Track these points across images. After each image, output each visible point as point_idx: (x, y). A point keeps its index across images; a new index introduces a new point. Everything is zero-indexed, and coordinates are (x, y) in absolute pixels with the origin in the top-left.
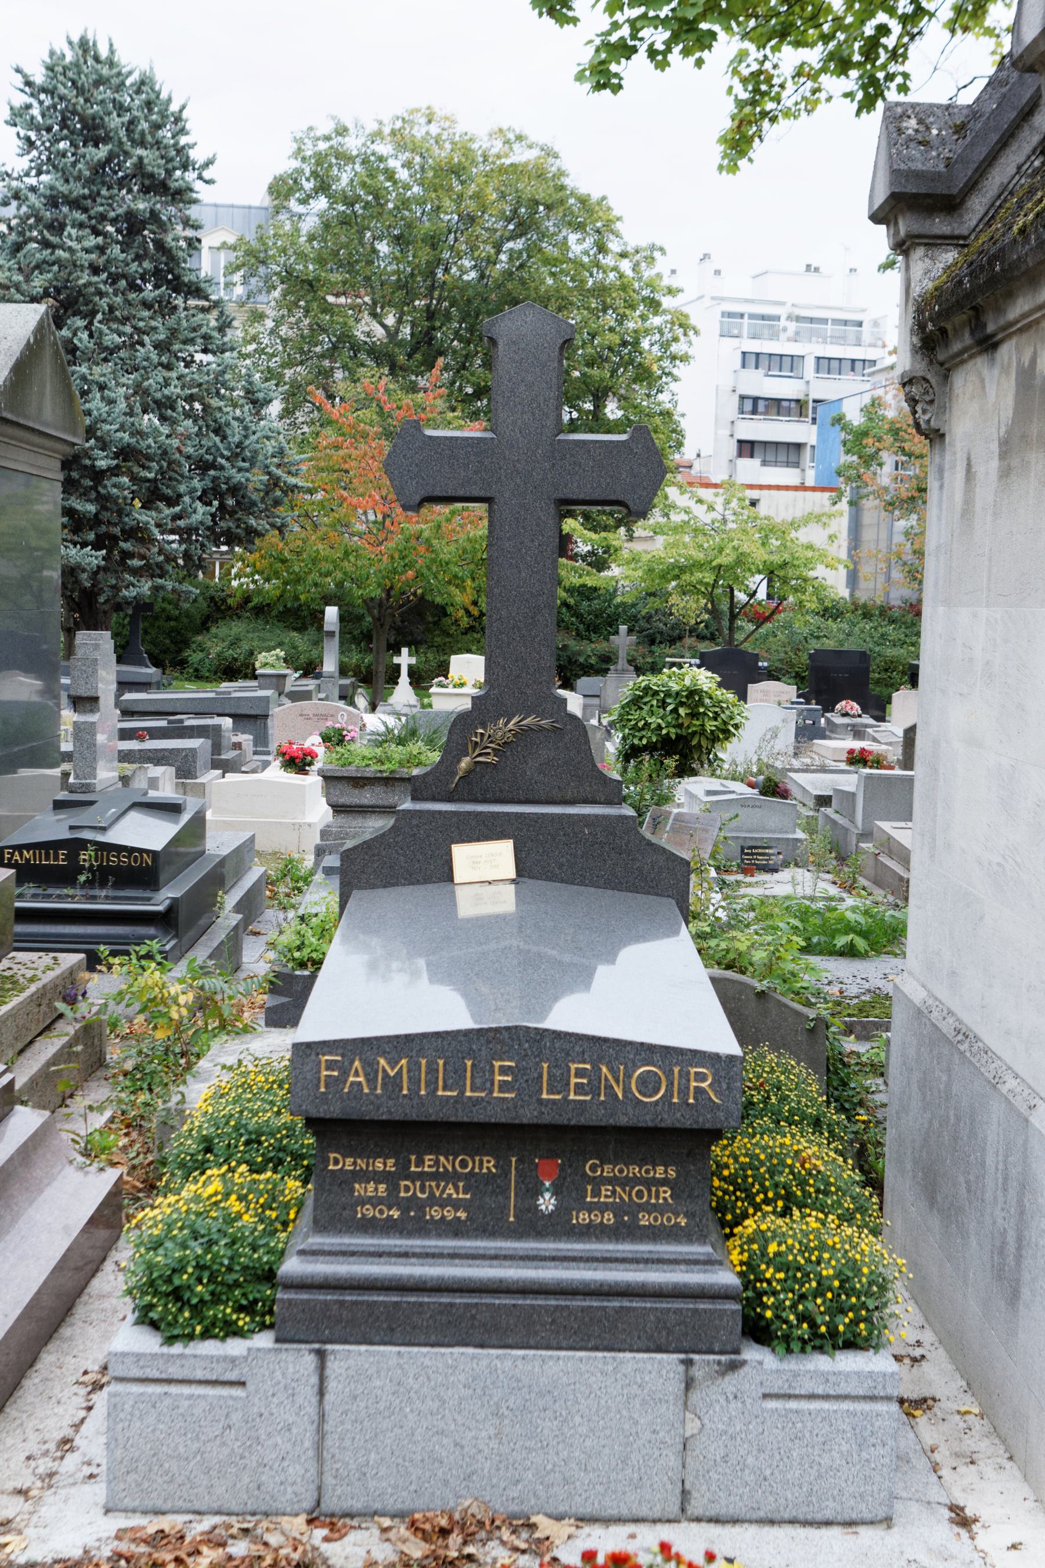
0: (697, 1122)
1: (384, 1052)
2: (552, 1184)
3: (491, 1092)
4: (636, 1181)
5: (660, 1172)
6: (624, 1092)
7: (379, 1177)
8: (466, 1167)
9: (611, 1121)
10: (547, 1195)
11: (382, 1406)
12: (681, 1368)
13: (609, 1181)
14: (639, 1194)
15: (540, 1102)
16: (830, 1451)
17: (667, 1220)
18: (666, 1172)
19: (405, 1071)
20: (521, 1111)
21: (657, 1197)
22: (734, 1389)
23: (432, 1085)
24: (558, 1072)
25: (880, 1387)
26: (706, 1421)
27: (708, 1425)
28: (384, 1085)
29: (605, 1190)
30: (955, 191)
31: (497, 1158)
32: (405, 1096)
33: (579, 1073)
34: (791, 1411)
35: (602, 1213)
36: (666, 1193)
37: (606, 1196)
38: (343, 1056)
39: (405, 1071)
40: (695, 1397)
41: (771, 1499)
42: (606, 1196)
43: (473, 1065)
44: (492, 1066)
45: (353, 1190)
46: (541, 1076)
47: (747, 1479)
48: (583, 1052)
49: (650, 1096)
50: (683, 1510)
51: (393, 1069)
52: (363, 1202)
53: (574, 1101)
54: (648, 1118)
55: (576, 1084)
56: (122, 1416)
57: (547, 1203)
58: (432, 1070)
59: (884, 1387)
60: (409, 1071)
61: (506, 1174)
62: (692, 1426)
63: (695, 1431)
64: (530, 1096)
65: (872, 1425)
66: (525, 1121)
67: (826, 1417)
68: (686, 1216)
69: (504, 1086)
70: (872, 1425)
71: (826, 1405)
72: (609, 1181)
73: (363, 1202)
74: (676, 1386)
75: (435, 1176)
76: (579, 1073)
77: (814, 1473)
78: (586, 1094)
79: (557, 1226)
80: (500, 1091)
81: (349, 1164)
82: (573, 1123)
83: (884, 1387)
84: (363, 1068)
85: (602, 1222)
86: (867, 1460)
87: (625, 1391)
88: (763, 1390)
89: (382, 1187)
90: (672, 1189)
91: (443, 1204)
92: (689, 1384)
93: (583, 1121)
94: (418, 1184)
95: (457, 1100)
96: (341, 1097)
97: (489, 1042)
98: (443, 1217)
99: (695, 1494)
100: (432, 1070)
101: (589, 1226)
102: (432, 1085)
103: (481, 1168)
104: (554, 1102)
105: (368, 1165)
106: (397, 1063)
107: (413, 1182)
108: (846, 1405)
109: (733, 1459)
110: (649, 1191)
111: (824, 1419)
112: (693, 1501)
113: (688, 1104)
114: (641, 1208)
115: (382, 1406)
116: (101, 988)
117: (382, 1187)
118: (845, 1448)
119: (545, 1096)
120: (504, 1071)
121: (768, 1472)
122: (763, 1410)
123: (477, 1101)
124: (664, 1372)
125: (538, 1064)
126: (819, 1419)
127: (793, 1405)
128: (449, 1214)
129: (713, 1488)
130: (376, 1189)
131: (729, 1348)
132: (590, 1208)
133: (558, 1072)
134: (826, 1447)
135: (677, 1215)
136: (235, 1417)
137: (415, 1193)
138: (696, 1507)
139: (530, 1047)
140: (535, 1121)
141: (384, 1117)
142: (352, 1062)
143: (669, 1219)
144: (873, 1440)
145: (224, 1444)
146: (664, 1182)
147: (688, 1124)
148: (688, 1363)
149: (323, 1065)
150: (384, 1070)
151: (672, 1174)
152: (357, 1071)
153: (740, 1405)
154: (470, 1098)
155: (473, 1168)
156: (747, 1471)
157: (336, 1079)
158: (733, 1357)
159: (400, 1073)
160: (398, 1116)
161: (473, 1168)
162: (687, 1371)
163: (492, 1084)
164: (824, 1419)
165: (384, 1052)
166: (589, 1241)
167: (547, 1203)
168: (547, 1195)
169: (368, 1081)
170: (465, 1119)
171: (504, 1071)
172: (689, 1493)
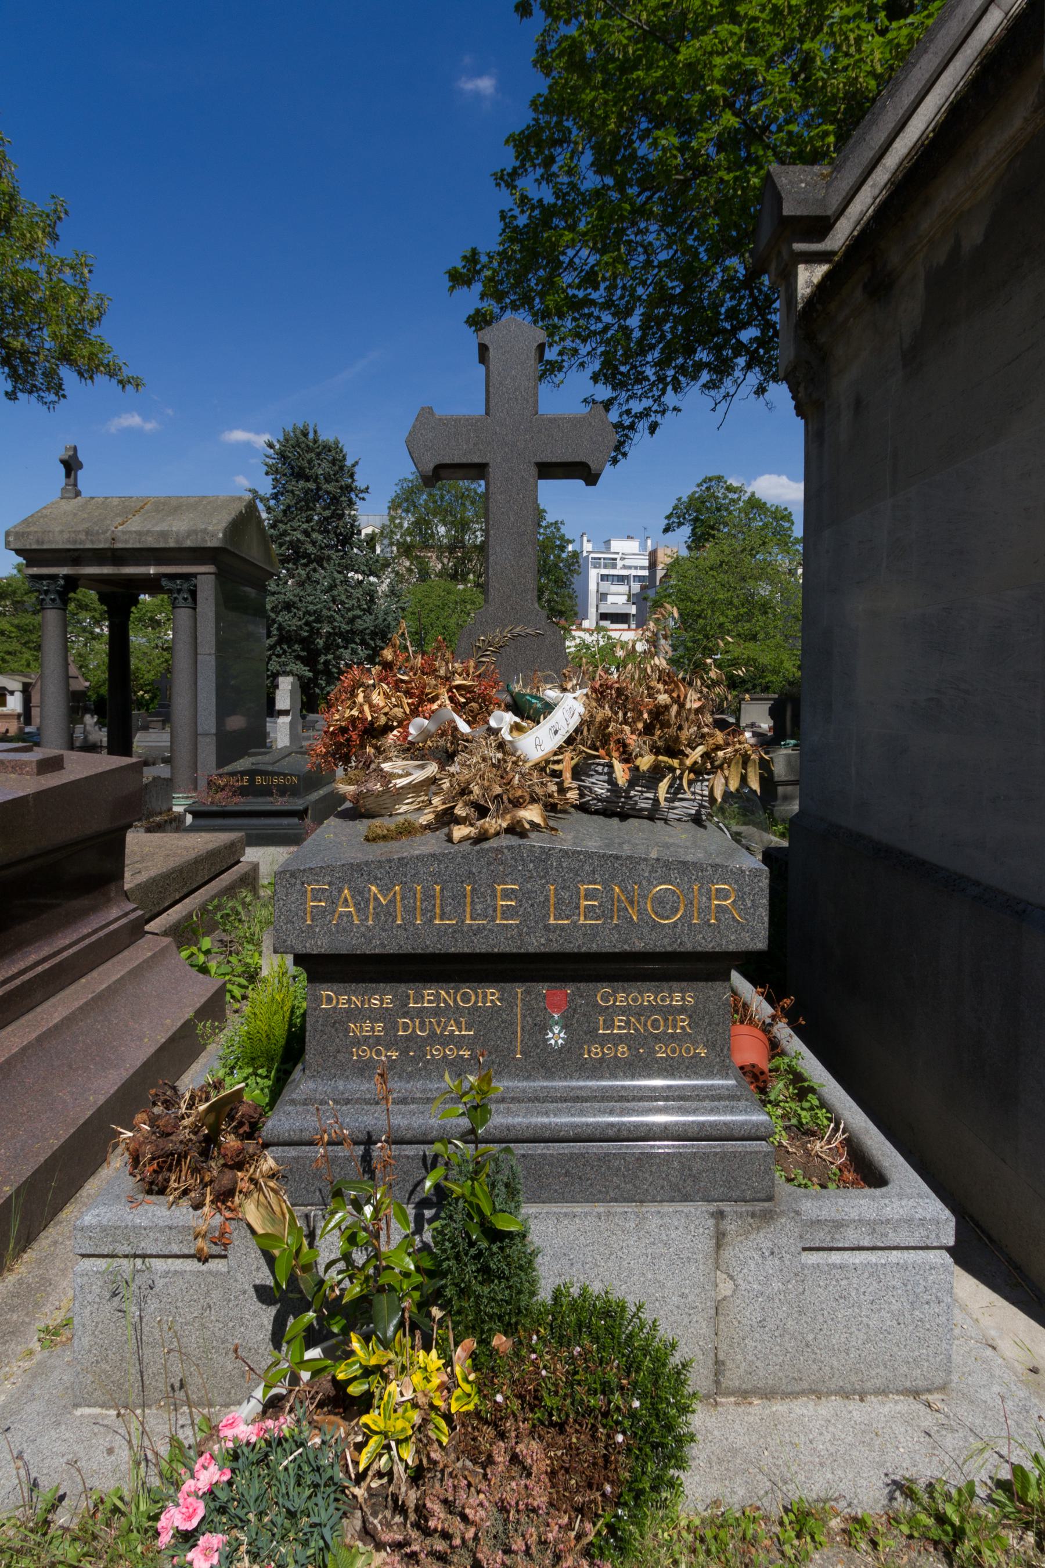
0: (721, 945)
1: (376, 878)
2: (562, 1017)
3: (494, 919)
4: (654, 1009)
5: (677, 1000)
6: (640, 913)
7: (375, 1015)
8: (469, 1001)
9: (626, 947)
10: (556, 1029)
11: (675, 287)
12: (711, 1222)
13: (623, 1011)
14: (655, 1024)
15: (547, 927)
16: (879, 1310)
17: (688, 1050)
18: (683, 999)
19: (398, 897)
20: (527, 939)
21: (675, 1027)
22: (770, 1244)
23: (429, 914)
24: (566, 895)
25: (933, 1236)
26: (740, 1282)
27: (743, 1285)
28: (377, 915)
29: (619, 1020)
30: (829, 213)
31: (502, 991)
32: (399, 926)
33: (590, 895)
34: (834, 1266)
35: (616, 1045)
36: (684, 1021)
37: (619, 1027)
38: (330, 884)
39: (398, 897)
40: (727, 1253)
41: (815, 1367)
42: (619, 1027)
43: (473, 890)
44: (494, 890)
45: (347, 1030)
46: (547, 900)
47: (788, 1345)
48: (593, 872)
49: (667, 918)
50: (717, 1383)
51: (385, 896)
52: (357, 1042)
53: (584, 925)
54: (666, 941)
55: (586, 907)
56: (89, 1298)
57: (556, 1037)
58: (428, 896)
59: (938, 1237)
60: (402, 899)
61: (512, 1006)
62: (726, 1288)
63: (729, 1293)
64: (536, 922)
65: (926, 1280)
66: (531, 950)
67: (874, 1271)
68: (706, 1046)
69: (507, 912)
70: (926, 1280)
71: (872, 1257)
72: (623, 1011)
73: (357, 1042)
74: (706, 1244)
75: (437, 1012)
76: (590, 895)
77: (862, 1336)
78: (597, 918)
79: (566, 1062)
80: (502, 919)
81: (343, 1002)
82: (583, 950)
83: (938, 1237)
84: (353, 897)
85: (616, 1056)
86: (921, 1320)
87: (650, 1251)
88: (802, 1245)
89: (379, 1026)
90: (690, 1017)
91: (447, 1041)
92: (720, 1239)
93: (594, 948)
94: (417, 1021)
95: (457, 929)
96: (330, 930)
97: (489, 864)
98: (445, 1056)
99: (729, 1364)
100: (428, 896)
101: (602, 1060)
102: (429, 914)
103: (484, 1003)
104: (562, 928)
105: (363, 1003)
106: (389, 890)
107: (411, 1019)
108: (895, 1256)
109: (771, 1325)
110: (666, 1020)
111: (871, 1275)
112: (727, 1374)
113: (710, 925)
114: (657, 1038)
115: (675, 287)
116: (252, 854)
117: (379, 1026)
118: (896, 1306)
119: (552, 921)
120: (507, 895)
121: (810, 1337)
122: (803, 1267)
123: (478, 931)
124: (692, 1227)
125: (543, 886)
126: (866, 1275)
127: (835, 1257)
128: (450, 1053)
129: (750, 1358)
130: (373, 1029)
131: (762, 1195)
132: (603, 1040)
133: (566, 895)
134: (875, 1307)
135: (695, 1043)
136: (216, 1295)
137: (414, 1031)
138: (732, 1379)
139: (536, 868)
140: (543, 949)
141: (377, 951)
142: (340, 891)
143: (688, 1050)
144: (927, 1297)
145: (203, 1326)
146: (682, 1010)
147: (709, 947)
148: (720, 1215)
149: (309, 895)
150: (376, 899)
151: (690, 1000)
152: (346, 900)
153: (777, 1262)
154: (471, 925)
155: (476, 1002)
156: (787, 1337)
157: (324, 910)
158: (766, 1204)
159: (392, 901)
160: (392, 949)
161: (476, 1002)
162: (717, 1225)
163: (495, 911)
164: (871, 1275)
165: (376, 878)
166: (602, 1078)
167: (556, 1037)
168: (556, 1029)
169: (358, 910)
170: (467, 950)
171: (507, 895)
172: (723, 1363)
